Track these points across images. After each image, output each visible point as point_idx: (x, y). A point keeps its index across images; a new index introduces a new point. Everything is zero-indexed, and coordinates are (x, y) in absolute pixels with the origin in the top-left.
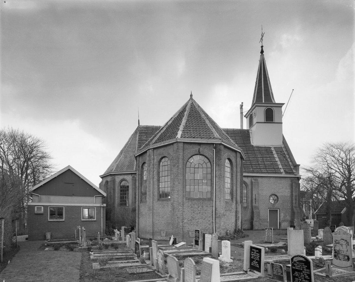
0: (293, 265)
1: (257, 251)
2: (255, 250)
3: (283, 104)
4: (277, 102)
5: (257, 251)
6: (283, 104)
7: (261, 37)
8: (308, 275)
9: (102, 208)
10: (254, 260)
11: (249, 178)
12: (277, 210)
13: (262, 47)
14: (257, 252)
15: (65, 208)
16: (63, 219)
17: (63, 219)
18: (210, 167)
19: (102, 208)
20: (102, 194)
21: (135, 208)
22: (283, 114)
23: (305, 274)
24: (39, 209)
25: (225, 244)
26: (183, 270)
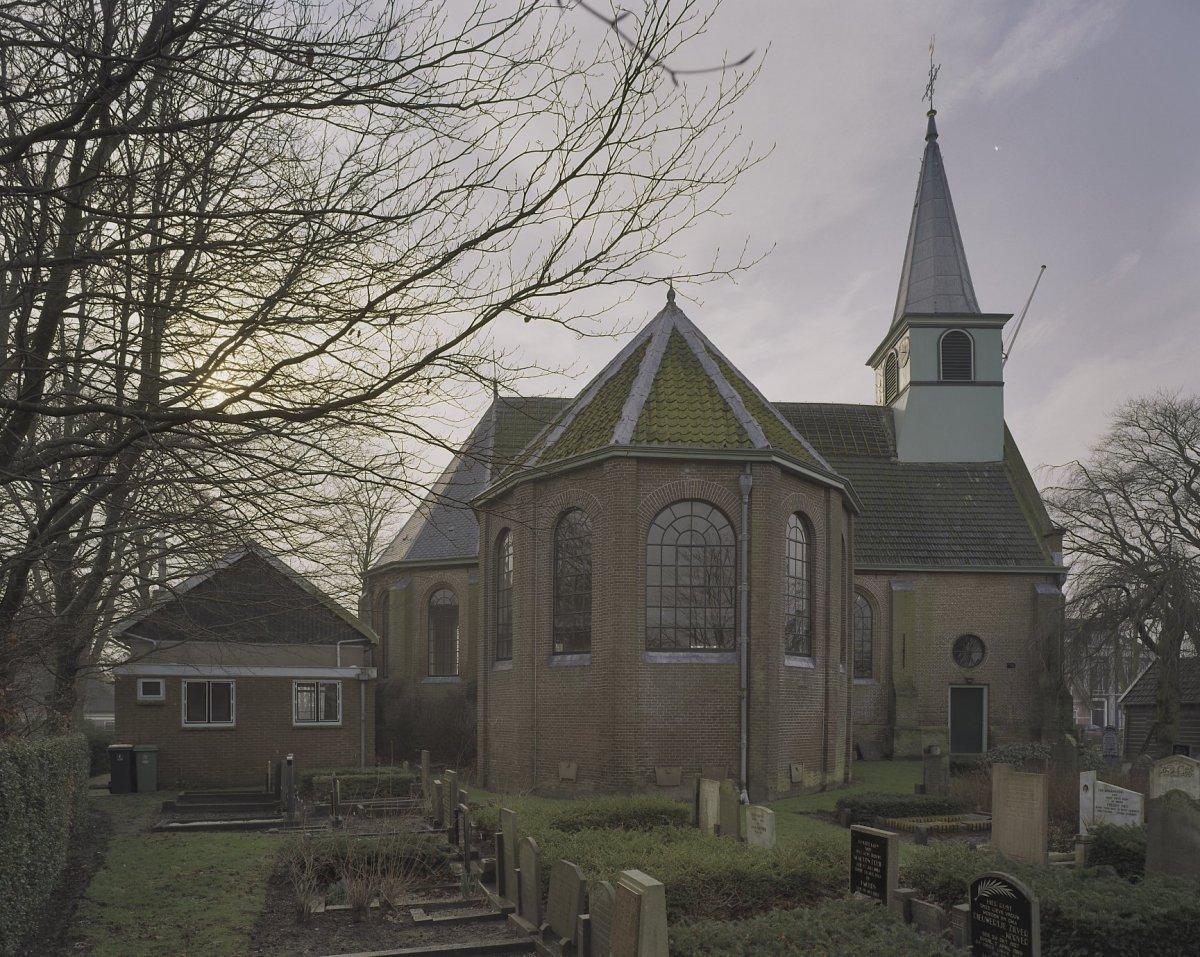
0: (975, 907)
1: (874, 846)
2: (867, 843)
3: (1009, 317)
4: (984, 309)
5: (874, 846)
6: (1009, 317)
7: (928, 82)
8: (1021, 947)
9: (363, 685)
10: (862, 877)
11: (880, 578)
12: (982, 689)
13: (932, 113)
14: (874, 851)
15: (237, 684)
16: (228, 719)
17: (228, 719)
18: (733, 543)
19: (363, 685)
20: (364, 637)
21: (476, 682)
22: (1005, 352)
23: (1013, 944)
24: (153, 688)
25: (759, 819)
26: (585, 920)
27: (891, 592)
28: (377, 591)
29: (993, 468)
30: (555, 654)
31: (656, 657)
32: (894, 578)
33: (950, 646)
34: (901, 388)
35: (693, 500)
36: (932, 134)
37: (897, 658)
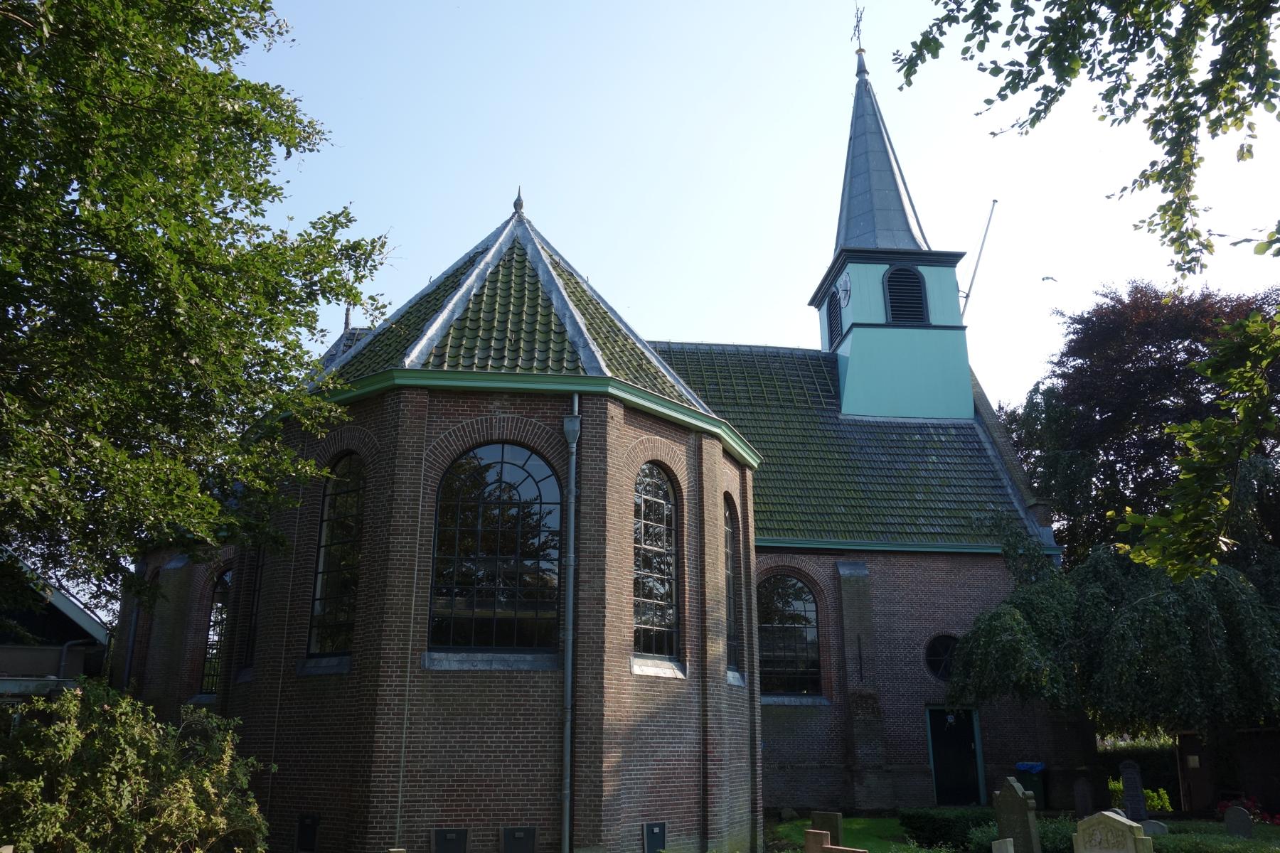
7: (861, 23)
11: (823, 559)
13: (860, 52)
27: (837, 578)
28: (151, 567)
29: (962, 430)
30: (310, 656)
31: (440, 661)
32: (842, 559)
33: (922, 651)
34: (845, 331)
35: (504, 442)
36: (862, 70)
37: (851, 666)
